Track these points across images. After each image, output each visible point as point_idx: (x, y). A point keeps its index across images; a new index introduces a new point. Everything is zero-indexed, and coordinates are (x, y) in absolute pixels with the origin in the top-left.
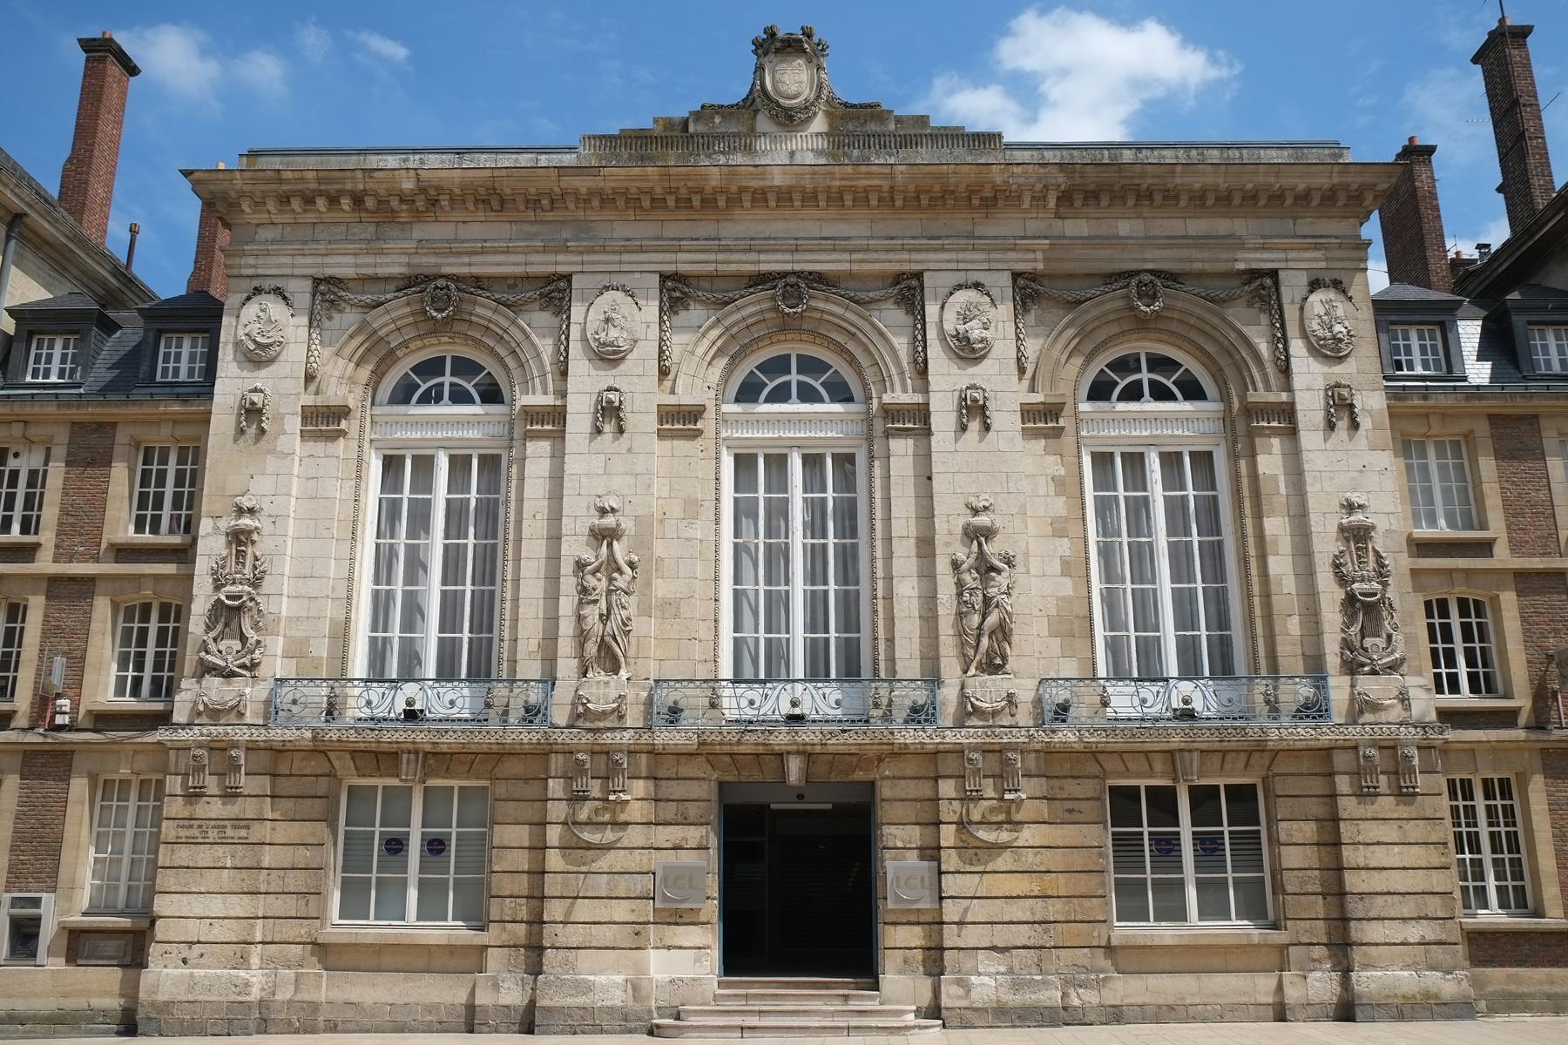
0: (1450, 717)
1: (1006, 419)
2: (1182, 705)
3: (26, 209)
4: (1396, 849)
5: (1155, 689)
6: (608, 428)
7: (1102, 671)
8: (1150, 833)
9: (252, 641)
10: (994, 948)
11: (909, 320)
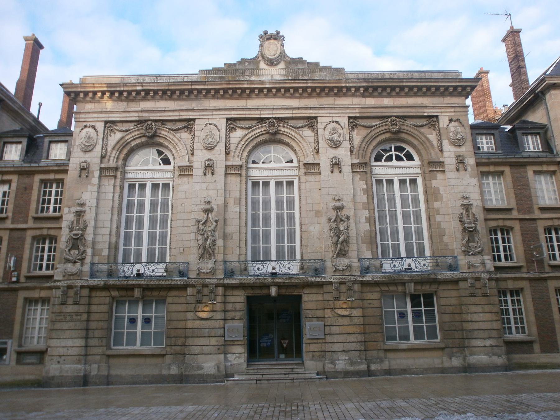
1: (347, 169)
2: (407, 267)
3: (4, 98)
4: (481, 315)
5: (398, 262)
7: (380, 256)
8: (425, 310)
10: (344, 351)
11: (313, 134)
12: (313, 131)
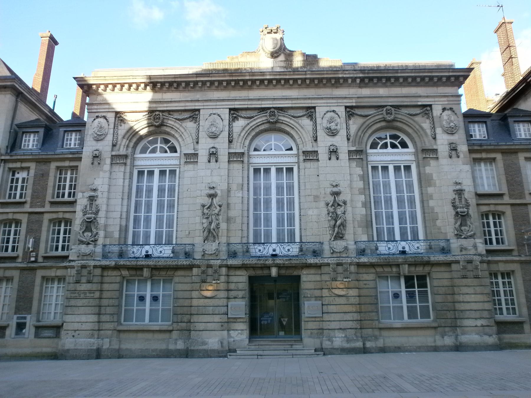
0: (489, 252)
1: (344, 155)
2: (402, 250)
4: (473, 296)
5: (393, 244)
6: (96, 163)
8: (418, 291)
9: (95, 233)
10: (341, 329)
11: (311, 123)
12: (311, 120)
